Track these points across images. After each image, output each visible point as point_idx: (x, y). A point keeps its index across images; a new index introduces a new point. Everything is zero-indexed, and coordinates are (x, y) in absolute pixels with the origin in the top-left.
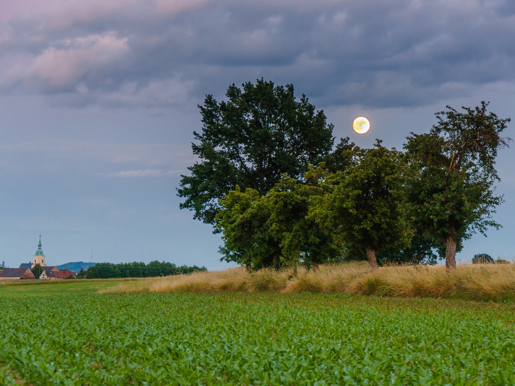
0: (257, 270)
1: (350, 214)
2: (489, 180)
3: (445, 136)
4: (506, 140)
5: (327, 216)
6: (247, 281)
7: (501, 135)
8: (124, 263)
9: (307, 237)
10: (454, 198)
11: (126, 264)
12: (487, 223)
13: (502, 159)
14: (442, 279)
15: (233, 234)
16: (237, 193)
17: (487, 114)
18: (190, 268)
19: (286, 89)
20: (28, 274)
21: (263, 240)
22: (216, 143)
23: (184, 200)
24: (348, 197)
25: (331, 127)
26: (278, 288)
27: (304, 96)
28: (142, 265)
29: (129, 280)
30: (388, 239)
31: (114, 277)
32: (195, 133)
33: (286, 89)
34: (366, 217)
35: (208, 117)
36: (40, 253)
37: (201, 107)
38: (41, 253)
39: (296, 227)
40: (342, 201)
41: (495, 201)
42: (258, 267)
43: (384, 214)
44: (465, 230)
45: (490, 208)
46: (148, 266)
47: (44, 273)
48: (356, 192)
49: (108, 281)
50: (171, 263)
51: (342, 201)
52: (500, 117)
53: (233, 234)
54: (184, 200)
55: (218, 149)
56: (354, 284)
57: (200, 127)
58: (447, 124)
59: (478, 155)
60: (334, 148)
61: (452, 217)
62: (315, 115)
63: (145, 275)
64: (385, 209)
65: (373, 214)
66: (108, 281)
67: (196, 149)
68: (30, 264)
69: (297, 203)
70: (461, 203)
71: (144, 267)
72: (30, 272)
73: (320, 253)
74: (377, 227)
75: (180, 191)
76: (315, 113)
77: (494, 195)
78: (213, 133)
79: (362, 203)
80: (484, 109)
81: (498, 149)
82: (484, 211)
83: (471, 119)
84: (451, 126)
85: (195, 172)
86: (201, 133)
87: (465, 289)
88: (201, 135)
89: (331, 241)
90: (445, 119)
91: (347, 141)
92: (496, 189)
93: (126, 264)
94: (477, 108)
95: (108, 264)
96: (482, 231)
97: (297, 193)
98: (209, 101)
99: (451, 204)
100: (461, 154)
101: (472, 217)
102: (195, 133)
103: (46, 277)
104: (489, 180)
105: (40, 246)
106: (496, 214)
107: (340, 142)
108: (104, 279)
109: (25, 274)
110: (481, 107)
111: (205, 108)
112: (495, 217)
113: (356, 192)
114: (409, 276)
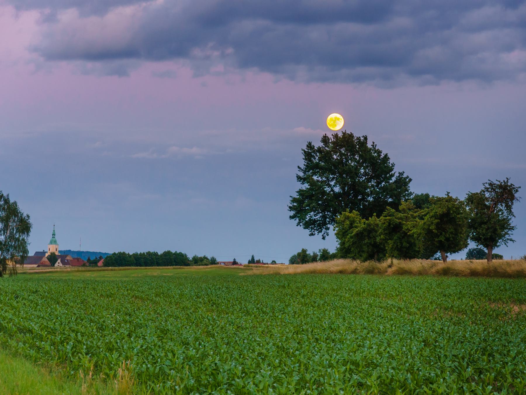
0: (364, 262)
1: (433, 232)
2: (510, 217)
3: (487, 195)
4: (518, 198)
5: (420, 234)
6: (358, 268)
7: (516, 195)
8: (139, 253)
9: (402, 243)
10: (492, 227)
11: (141, 253)
12: (508, 239)
13: (516, 207)
14: (486, 267)
15: (352, 240)
16: (347, 214)
17: (509, 184)
18: (201, 258)
19: (362, 139)
20: (44, 261)
21: (370, 244)
22: (314, 174)
23: (292, 213)
24: (432, 223)
25: (393, 165)
26: (381, 273)
27: (374, 143)
28: (156, 254)
29: (30, 269)
30: (452, 246)
31: (130, 266)
32: (299, 167)
33: (362, 139)
34: (441, 234)
35: (308, 156)
36: (53, 242)
37: (304, 150)
38: (55, 242)
39: (395, 238)
40: (429, 225)
41: (512, 228)
42: (365, 260)
43: (452, 233)
44: (497, 242)
45: (510, 232)
46: (161, 255)
47: (59, 261)
48: (437, 221)
49: (141, 269)
50: (183, 253)
51: (429, 225)
52: (516, 185)
53: (352, 240)
54: (292, 213)
55: (315, 178)
56: (434, 270)
57: (302, 164)
58: (488, 188)
59: (504, 205)
60: (394, 179)
61: (491, 236)
62: (382, 157)
63: (158, 264)
64: (452, 230)
65: (445, 232)
66: (167, 269)
67: (299, 178)
68: (44, 253)
69: (396, 224)
70: (496, 230)
71: (157, 257)
72: (47, 260)
73: (407, 252)
74: (447, 239)
75: (290, 207)
76: (382, 156)
77: (512, 225)
78: (311, 167)
79: (438, 226)
80: (507, 182)
81: (514, 201)
82: (506, 233)
83: (500, 187)
84: (490, 190)
85: (300, 195)
86: (303, 167)
87: (498, 272)
88: (302, 168)
89: (415, 246)
90: (487, 186)
91: (403, 174)
92: (513, 222)
93: (141, 253)
94: (504, 181)
95: (124, 253)
96: (505, 244)
97: (396, 218)
98: (310, 146)
99: (491, 230)
100: (496, 204)
101: (501, 237)
102: (299, 167)
103: (61, 265)
104: (510, 217)
105: (54, 235)
106: (513, 234)
107: (398, 175)
108: (139, 267)
109: (41, 262)
110: (506, 181)
111: (307, 150)
112: (512, 237)
113: (437, 221)
114: (467, 266)
